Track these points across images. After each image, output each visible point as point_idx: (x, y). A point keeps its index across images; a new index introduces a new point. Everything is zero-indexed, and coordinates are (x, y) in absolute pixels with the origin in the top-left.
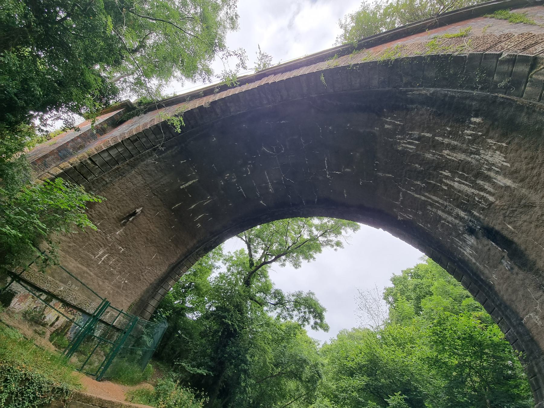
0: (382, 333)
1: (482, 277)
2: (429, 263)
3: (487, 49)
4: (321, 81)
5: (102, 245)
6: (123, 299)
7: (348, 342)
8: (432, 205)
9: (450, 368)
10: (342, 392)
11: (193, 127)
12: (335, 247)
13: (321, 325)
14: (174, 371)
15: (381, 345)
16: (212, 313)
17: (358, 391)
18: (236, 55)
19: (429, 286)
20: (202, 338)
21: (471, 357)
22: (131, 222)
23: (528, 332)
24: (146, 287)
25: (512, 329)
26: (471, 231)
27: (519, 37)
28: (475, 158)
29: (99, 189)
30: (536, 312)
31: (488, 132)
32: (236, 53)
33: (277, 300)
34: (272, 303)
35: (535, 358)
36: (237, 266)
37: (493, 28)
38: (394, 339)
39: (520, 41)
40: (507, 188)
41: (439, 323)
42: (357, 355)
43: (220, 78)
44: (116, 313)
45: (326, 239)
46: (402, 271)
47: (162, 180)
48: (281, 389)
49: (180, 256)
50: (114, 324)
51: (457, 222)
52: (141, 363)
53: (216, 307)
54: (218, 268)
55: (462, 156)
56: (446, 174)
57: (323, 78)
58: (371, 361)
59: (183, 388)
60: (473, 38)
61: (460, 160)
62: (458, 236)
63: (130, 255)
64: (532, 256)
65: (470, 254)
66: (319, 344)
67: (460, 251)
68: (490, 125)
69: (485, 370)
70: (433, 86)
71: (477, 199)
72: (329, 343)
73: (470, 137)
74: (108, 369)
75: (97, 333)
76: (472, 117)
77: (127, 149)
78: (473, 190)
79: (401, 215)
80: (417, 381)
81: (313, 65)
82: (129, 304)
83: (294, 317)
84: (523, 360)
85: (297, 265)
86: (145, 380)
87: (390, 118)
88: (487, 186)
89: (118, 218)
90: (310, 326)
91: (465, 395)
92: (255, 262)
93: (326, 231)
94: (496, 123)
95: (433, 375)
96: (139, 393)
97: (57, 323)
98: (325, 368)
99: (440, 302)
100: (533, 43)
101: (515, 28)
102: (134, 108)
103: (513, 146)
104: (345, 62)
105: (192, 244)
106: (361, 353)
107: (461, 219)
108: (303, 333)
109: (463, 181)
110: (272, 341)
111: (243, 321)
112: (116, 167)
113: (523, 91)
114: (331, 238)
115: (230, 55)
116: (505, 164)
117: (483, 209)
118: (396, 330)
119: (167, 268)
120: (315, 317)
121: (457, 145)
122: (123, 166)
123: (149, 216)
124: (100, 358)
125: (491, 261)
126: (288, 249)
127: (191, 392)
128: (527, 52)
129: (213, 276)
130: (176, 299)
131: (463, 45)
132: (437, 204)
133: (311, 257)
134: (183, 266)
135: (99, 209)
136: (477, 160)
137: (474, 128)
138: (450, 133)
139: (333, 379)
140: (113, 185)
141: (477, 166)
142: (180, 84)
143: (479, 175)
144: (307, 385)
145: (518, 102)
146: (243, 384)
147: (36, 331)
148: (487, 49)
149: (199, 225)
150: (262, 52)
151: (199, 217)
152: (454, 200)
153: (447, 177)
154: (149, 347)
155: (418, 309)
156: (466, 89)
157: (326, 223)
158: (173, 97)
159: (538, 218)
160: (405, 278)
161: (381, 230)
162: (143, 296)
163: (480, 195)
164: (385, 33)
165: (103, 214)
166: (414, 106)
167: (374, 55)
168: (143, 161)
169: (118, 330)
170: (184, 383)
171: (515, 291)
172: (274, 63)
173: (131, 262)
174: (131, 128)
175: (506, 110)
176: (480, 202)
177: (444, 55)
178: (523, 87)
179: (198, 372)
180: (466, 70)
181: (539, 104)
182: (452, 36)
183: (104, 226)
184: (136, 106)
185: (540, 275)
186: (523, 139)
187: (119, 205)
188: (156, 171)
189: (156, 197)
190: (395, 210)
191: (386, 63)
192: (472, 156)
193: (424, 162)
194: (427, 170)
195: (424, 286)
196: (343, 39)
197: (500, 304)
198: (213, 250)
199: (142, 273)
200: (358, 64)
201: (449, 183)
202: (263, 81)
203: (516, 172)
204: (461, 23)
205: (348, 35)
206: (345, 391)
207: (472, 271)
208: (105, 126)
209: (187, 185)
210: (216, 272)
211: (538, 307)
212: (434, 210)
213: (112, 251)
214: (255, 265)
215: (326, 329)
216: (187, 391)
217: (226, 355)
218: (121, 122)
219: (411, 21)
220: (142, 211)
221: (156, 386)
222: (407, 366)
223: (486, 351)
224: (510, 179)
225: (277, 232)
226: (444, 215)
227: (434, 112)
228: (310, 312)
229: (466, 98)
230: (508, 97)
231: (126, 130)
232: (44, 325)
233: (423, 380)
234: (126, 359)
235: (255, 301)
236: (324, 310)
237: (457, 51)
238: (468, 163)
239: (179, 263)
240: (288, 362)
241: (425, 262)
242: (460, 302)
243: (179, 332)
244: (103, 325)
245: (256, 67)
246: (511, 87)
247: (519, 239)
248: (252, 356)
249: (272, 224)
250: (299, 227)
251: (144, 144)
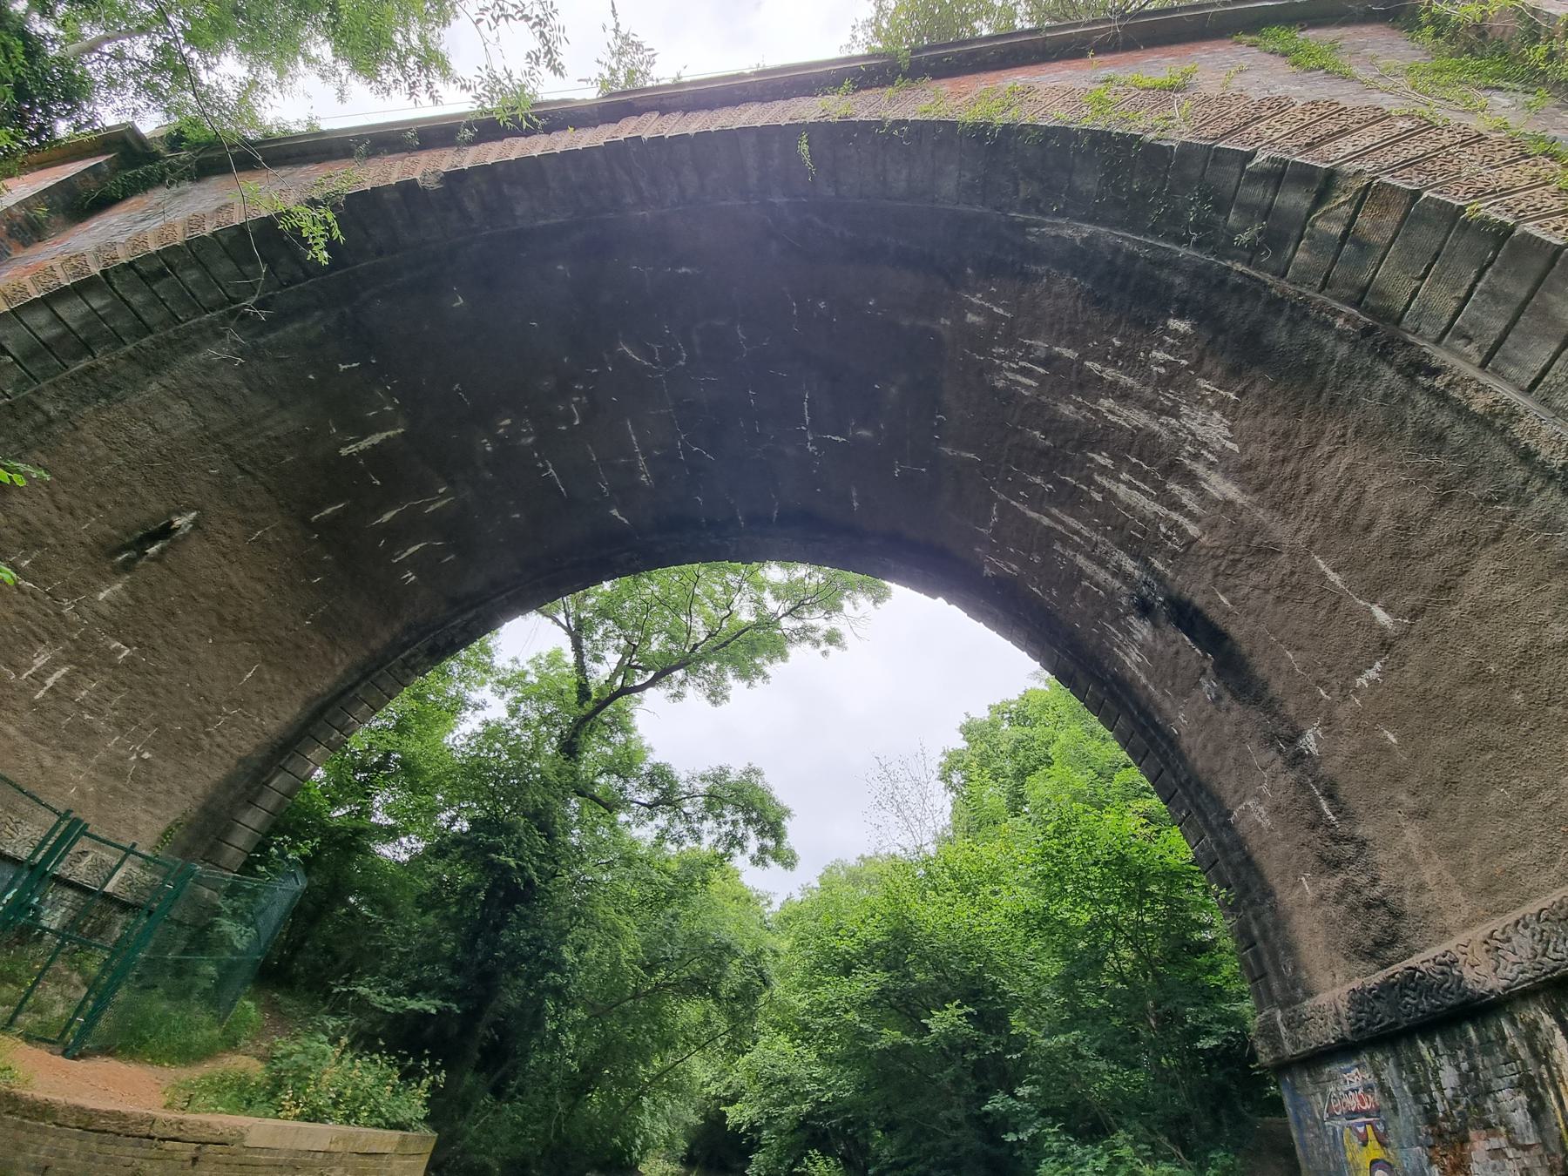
0: (926, 862)
1: (1157, 719)
2: (1051, 686)
3: (1225, 135)
4: (799, 156)
5: (45, 636)
7: (846, 891)
8: (1064, 540)
9: (1072, 933)
10: (823, 1015)
11: (380, 253)
12: (824, 646)
13: (777, 853)
14: (334, 1013)
15: (925, 892)
16: (458, 840)
17: (861, 1008)
18: (527, 18)
19: (1047, 744)
20: (424, 913)
21: (1119, 904)
22: (152, 559)
23: (1240, 843)
24: (225, 771)
25: (1207, 837)
26: (1145, 609)
27: (1303, 111)
28: (1168, 424)
29: (20, 440)
30: (1260, 797)
31: (1200, 360)
32: (527, 12)
33: (656, 793)
34: (642, 801)
35: (1252, 903)
36: (539, 699)
37: (1248, 76)
38: (954, 877)
39: (1306, 122)
40: (1229, 503)
41: (1058, 832)
42: (863, 922)
43: (472, 93)
44: (114, 855)
45: (799, 624)
46: (990, 707)
47: (269, 422)
48: (661, 1027)
49: (345, 671)
50: (109, 888)
51: (1117, 584)
52: (217, 998)
53: (472, 821)
54: (477, 707)
55: (1140, 418)
56: (1102, 462)
57: (806, 147)
58: (895, 934)
59: (360, 1058)
60: (1196, 97)
61: (1136, 427)
62: (1116, 619)
64: (1262, 671)
65: (1138, 665)
66: (770, 903)
67: (1118, 656)
68: (1208, 343)
69: (1145, 930)
70: (1090, 220)
71: (1163, 530)
72: (798, 898)
73: (1162, 370)
74: (101, 1024)
75: (53, 919)
76: (1170, 316)
77: (127, 303)
78: (1157, 507)
79: (991, 564)
80: (998, 970)
81: (780, 104)
82: (162, 827)
83: (704, 836)
84: (1230, 908)
85: (716, 695)
86: (232, 1045)
87: (979, 295)
88: (1187, 498)
89: (102, 546)
90: (747, 857)
91: (1100, 991)
92: (593, 690)
93: (801, 603)
94: (1221, 338)
95: (1036, 952)
96: (212, 1083)
98: (782, 961)
99: (1067, 780)
100: (1336, 130)
101: (1302, 82)
102: (154, 157)
103: (1250, 403)
104: (871, 109)
105: (386, 636)
106: (873, 916)
107: (1125, 577)
108: (730, 876)
109: (1138, 483)
110: (642, 903)
111: (554, 855)
112: (84, 363)
113: (1290, 261)
114: (814, 623)
115: (506, 17)
116: (1229, 445)
117: (1174, 555)
118: (961, 854)
120: (761, 833)
121: (1132, 388)
122: (113, 362)
123: (224, 540)
124: (70, 992)
125: (1179, 680)
126: (692, 651)
127: (389, 1065)
128: (1316, 156)
129: (464, 730)
130: (334, 803)
131: (1170, 113)
132: (1075, 538)
133: (759, 672)
134: (357, 701)
135: (21, 511)
136: (1173, 432)
137: (1173, 345)
138: (1119, 353)
139: (800, 985)
140: (77, 428)
141: (1170, 445)
142: (331, 89)
143: (1173, 469)
144: (732, 1007)
145: (1273, 291)
146: (550, 1026)
148: (1225, 135)
149: (410, 576)
150: (623, 30)
151: (411, 550)
152: (1114, 528)
153: (1103, 470)
154: (242, 953)
155: (1016, 802)
156: (1166, 238)
157: (803, 580)
158: (304, 136)
159: (1283, 581)
160: (994, 725)
161: (941, 601)
163: (1171, 519)
164: (989, 38)
165: (39, 525)
166: (1041, 269)
167: (951, 103)
168: (192, 349)
169: (125, 907)
170: (364, 1043)
171: (1220, 750)
172: (663, 72)
173: (161, 692)
174: (139, 227)
175: (1246, 306)
176: (1169, 538)
177: (1123, 135)
178: (1290, 251)
179: (410, 1007)
180: (1170, 187)
181: (1321, 298)
182: (1148, 83)
183: (47, 570)
184: (160, 148)
185: (1276, 714)
186: (1273, 385)
187: (103, 500)
188: (246, 391)
189: (249, 479)
190: (978, 549)
191: (979, 132)
192: (1163, 419)
193: (1056, 425)
194: (1061, 447)
195: (1035, 744)
196: (871, 34)
197: (1188, 781)
198: (463, 653)
199: (206, 726)
200: (905, 122)
201: (1107, 485)
202: (625, 130)
203: (1250, 466)
204: (1176, 49)
205: (885, 25)
206: (828, 1011)
207: (1137, 704)
208: (42, 212)
209: (364, 444)
210: (471, 718)
211: (1264, 787)
212: (1069, 553)
213: (84, 657)
214: (594, 697)
215: (788, 861)
216: (375, 1062)
217: (501, 954)
218: (103, 203)
219: (1055, 19)
220: (196, 524)
221: (268, 1059)
222: (979, 937)
223: (1154, 888)
224: (1236, 482)
225: (663, 602)
226: (1089, 567)
227: (1088, 291)
228: (748, 821)
229: (1161, 264)
230: (1253, 273)
231: (120, 233)
233: (1012, 966)
234: (161, 990)
235: (593, 798)
236: (787, 812)
237: (1154, 128)
238: (1153, 436)
239: (343, 693)
240: (682, 956)
241: (1043, 683)
242: (1111, 778)
243: (352, 900)
244: (70, 894)
245: (601, 75)
246: (1264, 249)
247: (1237, 631)
248: (581, 948)
249: (649, 578)
250: (727, 587)
251: (194, 290)
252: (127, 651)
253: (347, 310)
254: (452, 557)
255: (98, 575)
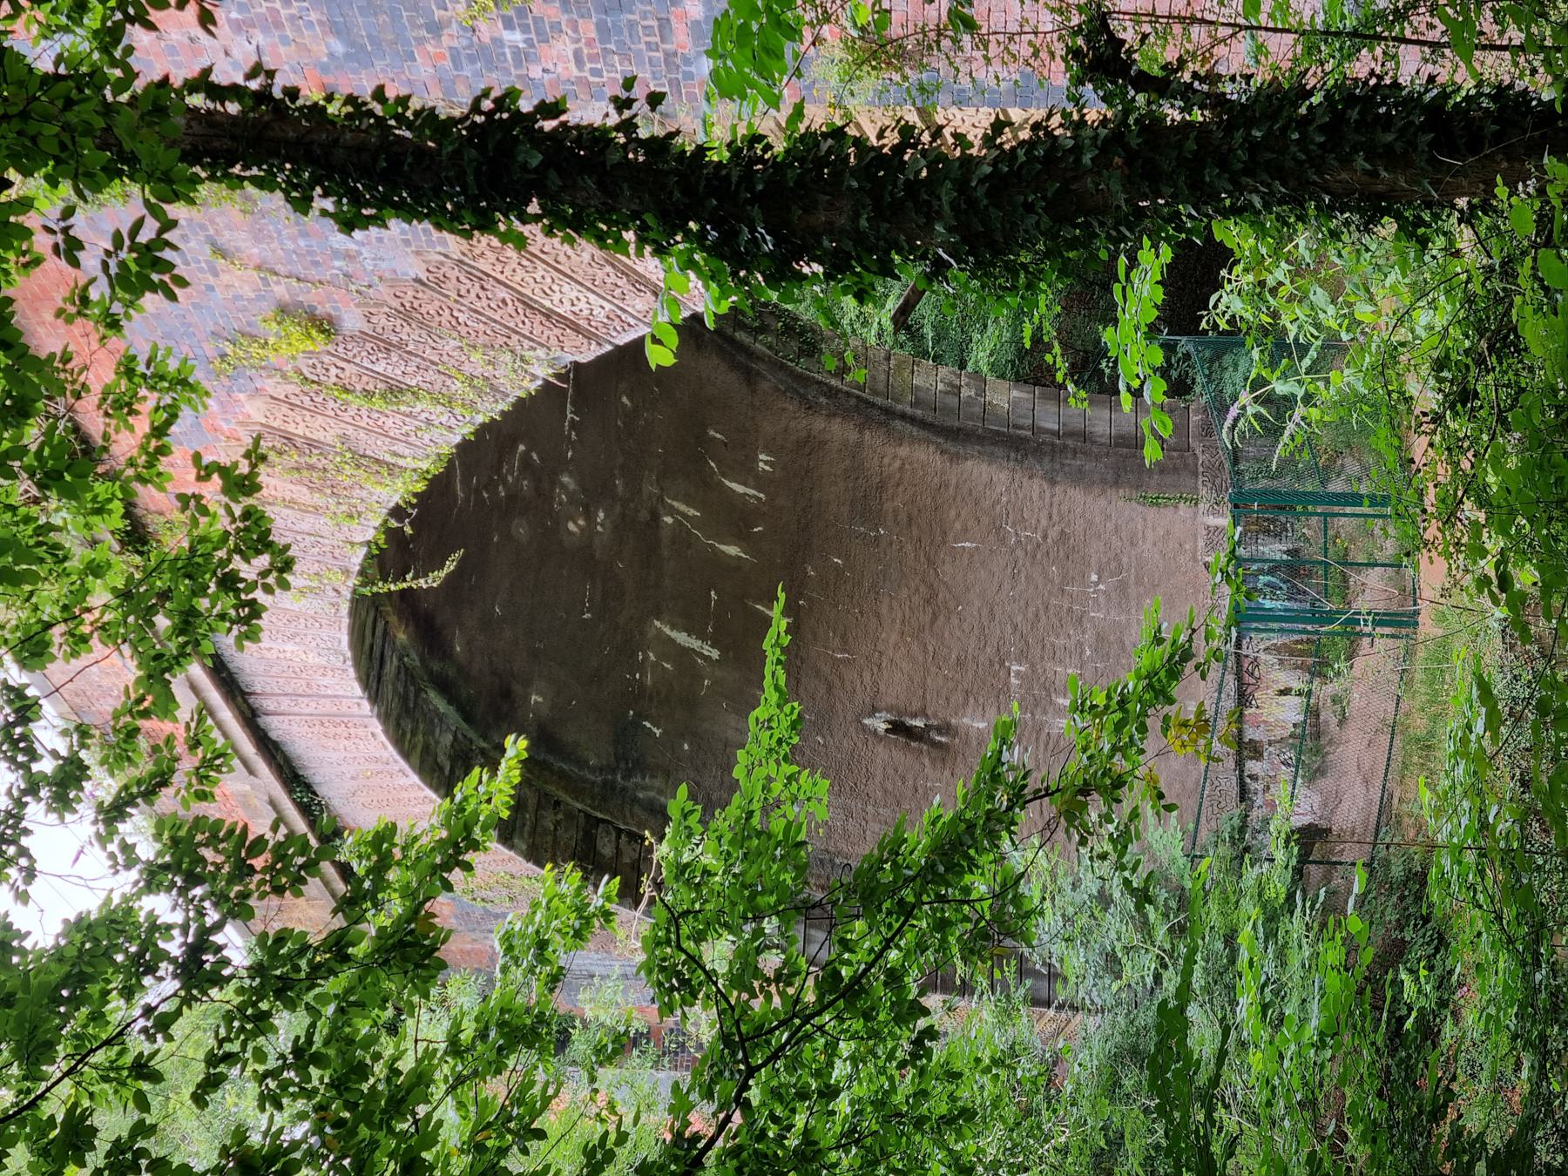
5: (1043, 737)
6: (1148, 545)
22: (927, 716)
24: (1071, 492)
63: (1014, 633)
82: (1151, 513)
97: (1296, 685)
119: (969, 463)
147: (1343, 721)
149: (764, 462)
162: (1104, 481)
173: (1031, 609)
187: (909, 793)
209: (694, 643)
220: (874, 710)
232: (1312, 712)
252: (1014, 668)
253: (619, 777)
254: (712, 433)
255: (967, 743)
